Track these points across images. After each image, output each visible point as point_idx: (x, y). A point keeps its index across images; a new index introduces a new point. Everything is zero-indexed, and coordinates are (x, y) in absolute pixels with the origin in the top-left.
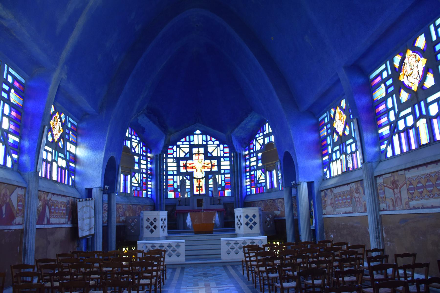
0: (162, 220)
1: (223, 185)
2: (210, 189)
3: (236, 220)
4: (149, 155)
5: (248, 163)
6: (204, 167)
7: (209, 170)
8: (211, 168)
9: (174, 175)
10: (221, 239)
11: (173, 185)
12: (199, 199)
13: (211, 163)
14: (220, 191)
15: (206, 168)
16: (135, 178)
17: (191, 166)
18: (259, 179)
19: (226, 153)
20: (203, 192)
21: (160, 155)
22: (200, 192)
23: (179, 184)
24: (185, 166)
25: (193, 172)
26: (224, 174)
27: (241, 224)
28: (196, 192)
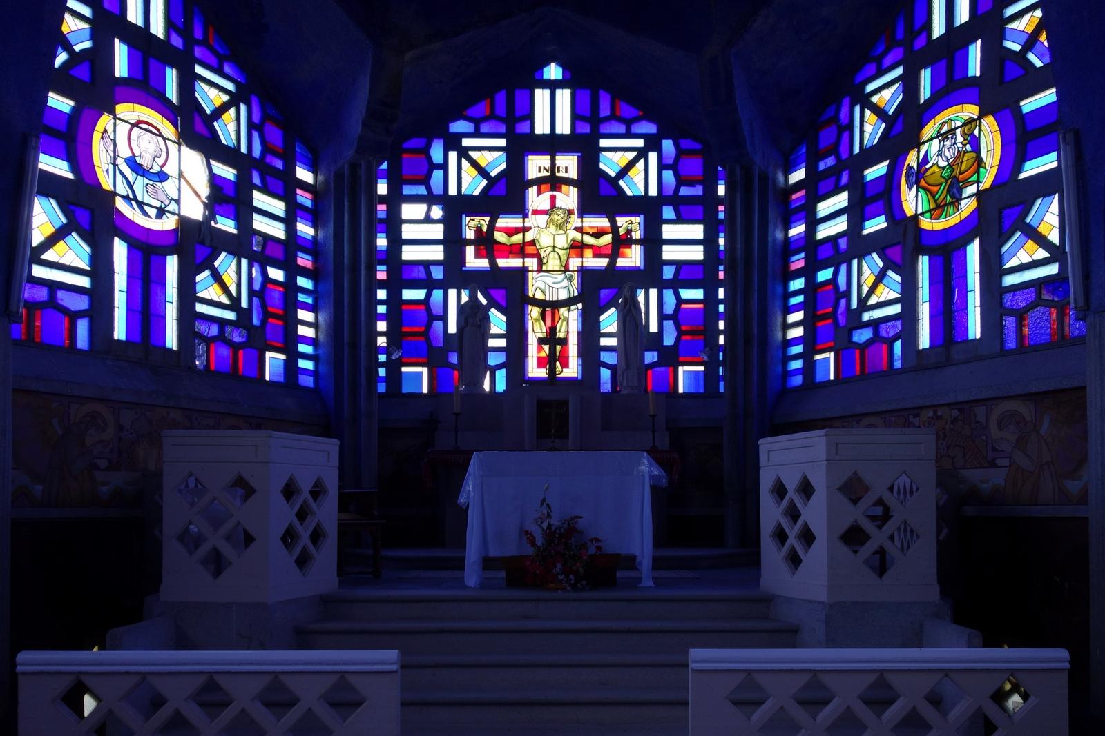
0: (289, 491)
1: (669, 340)
3: (770, 513)
4: (304, 175)
5: (798, 230)
6: (577, 248)
7: (603, 262)
9: (429, 284)
10: (695, 653)
13: (614, 228)
14: (652, 365)
15: (588, 253)
16: (217, 277)
17: (517, 238)
18: (863, 302)
20: (572, 370)
21: (354, 166)
22: (552, 371)
24: (486, 243)
25: (524, 271)
26: (676, 284)
27: (781, 536)
28: (535, 371)
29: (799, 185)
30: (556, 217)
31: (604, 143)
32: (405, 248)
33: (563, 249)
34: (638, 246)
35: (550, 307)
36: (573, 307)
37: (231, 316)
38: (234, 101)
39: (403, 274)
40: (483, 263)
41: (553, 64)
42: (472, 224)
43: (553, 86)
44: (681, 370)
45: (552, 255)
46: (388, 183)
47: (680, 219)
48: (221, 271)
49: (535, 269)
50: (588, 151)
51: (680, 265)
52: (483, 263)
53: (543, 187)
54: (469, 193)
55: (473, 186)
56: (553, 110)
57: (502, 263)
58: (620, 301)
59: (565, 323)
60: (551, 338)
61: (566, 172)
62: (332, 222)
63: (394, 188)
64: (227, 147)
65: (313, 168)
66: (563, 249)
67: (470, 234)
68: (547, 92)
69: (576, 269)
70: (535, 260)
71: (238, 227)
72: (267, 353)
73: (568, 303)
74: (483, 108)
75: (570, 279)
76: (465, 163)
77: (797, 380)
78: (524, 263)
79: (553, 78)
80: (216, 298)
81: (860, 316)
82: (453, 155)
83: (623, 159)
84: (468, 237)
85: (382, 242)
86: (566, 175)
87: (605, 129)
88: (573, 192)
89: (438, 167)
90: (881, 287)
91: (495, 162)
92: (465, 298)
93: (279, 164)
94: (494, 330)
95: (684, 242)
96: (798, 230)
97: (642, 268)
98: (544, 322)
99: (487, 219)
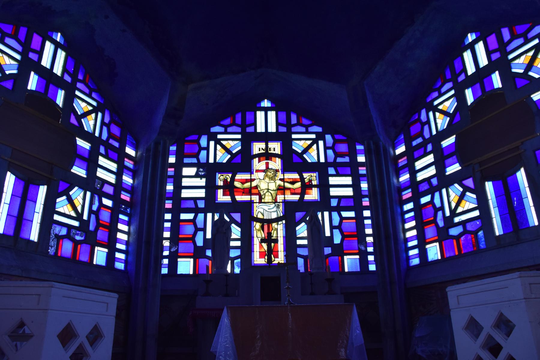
1: (337, 240)
2: (300, 251)
4: (130, 151)
5: (405, 177)
6: (282, 190)
7: (296, 197)
8: (303, 193)
9: (196, 211)
11: (192, 239)
12: (269, 280)
13: (302, 179)
14: (329, 255)
15: (288, 192)
17: (247, 185)
19: (342, 155)
21: (157, 144)
22: (270, 260)
23: (209, 236)
24: (229, 188)
25: (251, 202)
26: (339, 209)
28: (258, 260)
29: (402, 155)
30: (269, 173)
31: (294, 136)
32: (183, 191)
33: (274, 190)
34: (316, 189)
35: (266, 222)
36: (280, 223)
37: (76, 224)
38: (95, 110)
39: (180, 204)
40: (228, 199)
41: (266, 100)
42: (222, 178)
43: (266, 110)
44: (346, 258)
45: (267, 194)
46: (176, 157)
47: (338, 174)
48: (73, 197)
49: (258, 201)
50: (285, 139)
51: (340, 198)
52: (228, 199)
53: (262, 158)
54: (220, 161)
55: (223, 158)
56: (266, 121)
57: (239, 198)
58: (307, 219)
59: (275, 232)
60: (269, 240)
61: (274, 150)
62: (142, 175)
63: (180, 156)
64: (88, 132)
65: (135, 148)
66: (274, 190)
67: (220, 183)
68: (263, 113)
69: (281, 201)
70: (258, 197)
71: (87, 174)
72: (96, 247)
73: (277, 220)
74: (227, 121)
75: (278, 207)
76: (219, 147)
77: (416, 261)
78: (251, 198)
79: (266, 106)
80: (67, 213)
81: (453, 220)
82: (212, 143)
83: (304, 144)
84: (219, 185)
85: (170, 187)
86: (274, 152)
87: (294, 129)
88: (278, 161)
89: (204, 149)
90: (463, 202)
91: (235, 146)
92: (216, 217)
93: (116, 144)
94: (233, 236)
95: (341, 186)
96: (405, 177)
97: (319, 200)
98: (263, 231)
99: (230, 175)
